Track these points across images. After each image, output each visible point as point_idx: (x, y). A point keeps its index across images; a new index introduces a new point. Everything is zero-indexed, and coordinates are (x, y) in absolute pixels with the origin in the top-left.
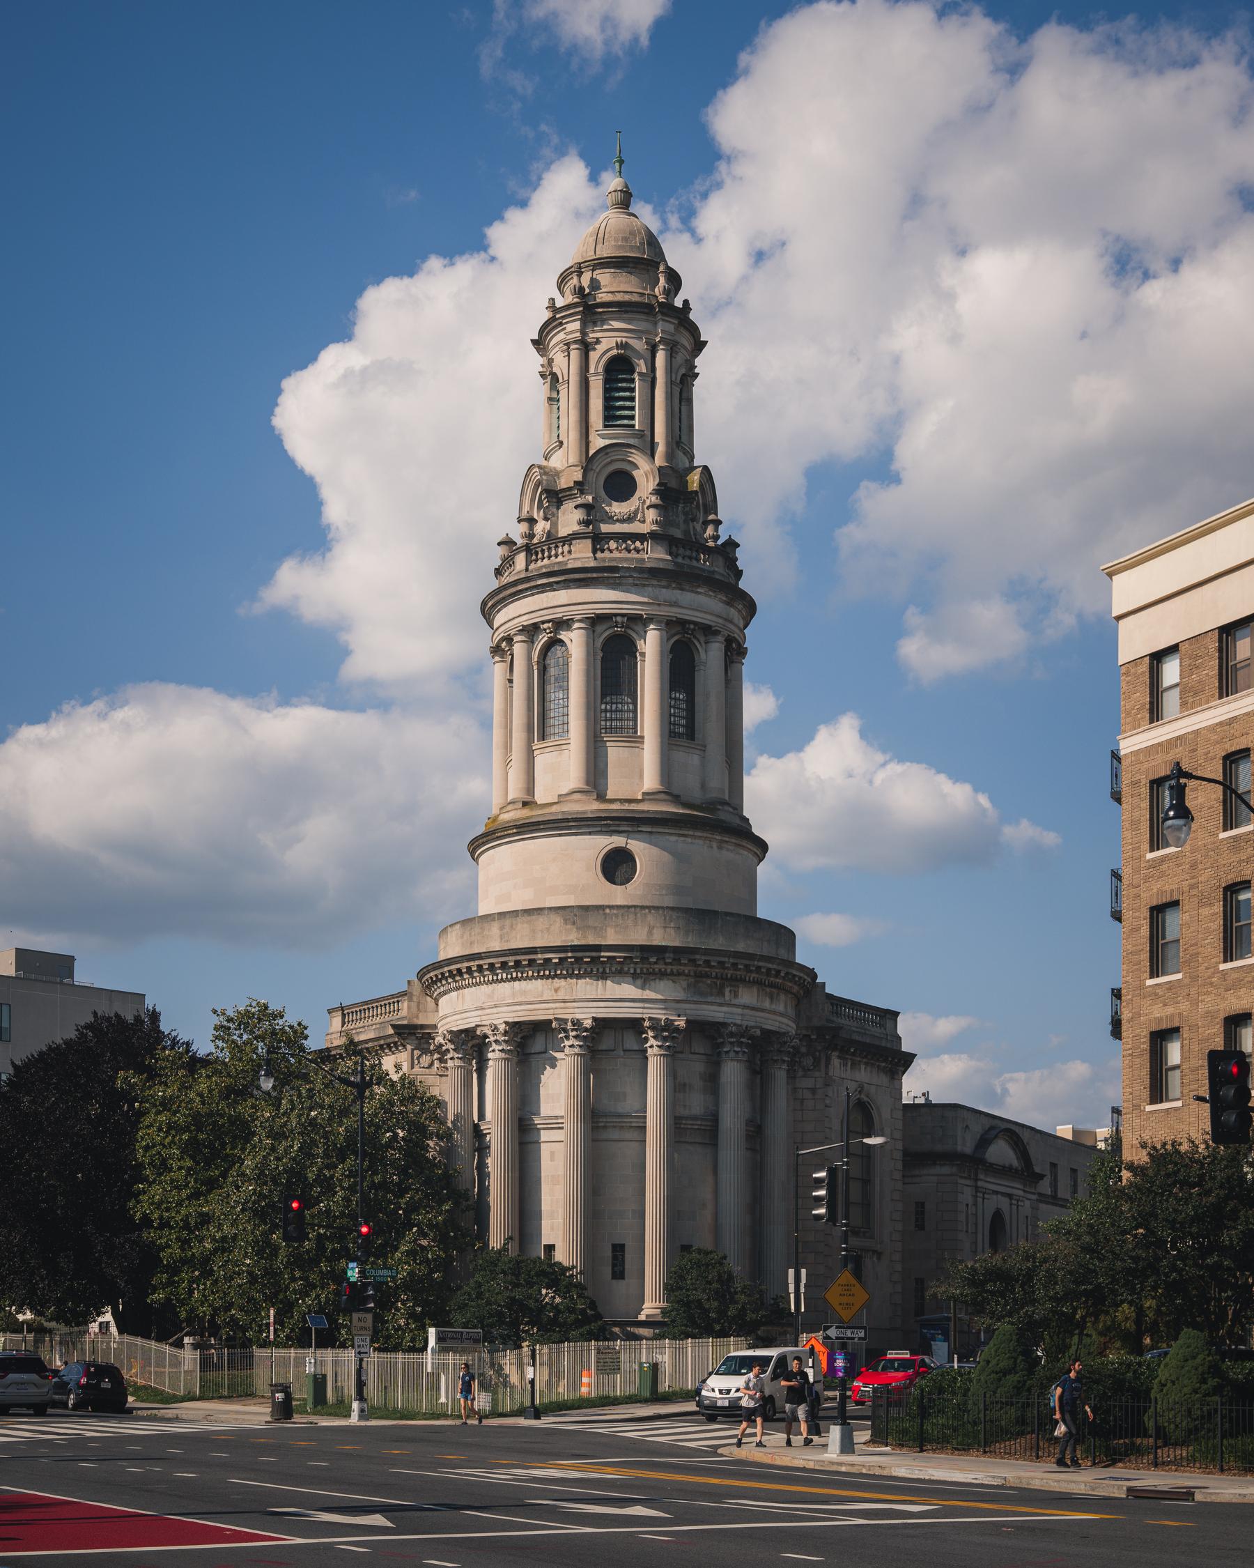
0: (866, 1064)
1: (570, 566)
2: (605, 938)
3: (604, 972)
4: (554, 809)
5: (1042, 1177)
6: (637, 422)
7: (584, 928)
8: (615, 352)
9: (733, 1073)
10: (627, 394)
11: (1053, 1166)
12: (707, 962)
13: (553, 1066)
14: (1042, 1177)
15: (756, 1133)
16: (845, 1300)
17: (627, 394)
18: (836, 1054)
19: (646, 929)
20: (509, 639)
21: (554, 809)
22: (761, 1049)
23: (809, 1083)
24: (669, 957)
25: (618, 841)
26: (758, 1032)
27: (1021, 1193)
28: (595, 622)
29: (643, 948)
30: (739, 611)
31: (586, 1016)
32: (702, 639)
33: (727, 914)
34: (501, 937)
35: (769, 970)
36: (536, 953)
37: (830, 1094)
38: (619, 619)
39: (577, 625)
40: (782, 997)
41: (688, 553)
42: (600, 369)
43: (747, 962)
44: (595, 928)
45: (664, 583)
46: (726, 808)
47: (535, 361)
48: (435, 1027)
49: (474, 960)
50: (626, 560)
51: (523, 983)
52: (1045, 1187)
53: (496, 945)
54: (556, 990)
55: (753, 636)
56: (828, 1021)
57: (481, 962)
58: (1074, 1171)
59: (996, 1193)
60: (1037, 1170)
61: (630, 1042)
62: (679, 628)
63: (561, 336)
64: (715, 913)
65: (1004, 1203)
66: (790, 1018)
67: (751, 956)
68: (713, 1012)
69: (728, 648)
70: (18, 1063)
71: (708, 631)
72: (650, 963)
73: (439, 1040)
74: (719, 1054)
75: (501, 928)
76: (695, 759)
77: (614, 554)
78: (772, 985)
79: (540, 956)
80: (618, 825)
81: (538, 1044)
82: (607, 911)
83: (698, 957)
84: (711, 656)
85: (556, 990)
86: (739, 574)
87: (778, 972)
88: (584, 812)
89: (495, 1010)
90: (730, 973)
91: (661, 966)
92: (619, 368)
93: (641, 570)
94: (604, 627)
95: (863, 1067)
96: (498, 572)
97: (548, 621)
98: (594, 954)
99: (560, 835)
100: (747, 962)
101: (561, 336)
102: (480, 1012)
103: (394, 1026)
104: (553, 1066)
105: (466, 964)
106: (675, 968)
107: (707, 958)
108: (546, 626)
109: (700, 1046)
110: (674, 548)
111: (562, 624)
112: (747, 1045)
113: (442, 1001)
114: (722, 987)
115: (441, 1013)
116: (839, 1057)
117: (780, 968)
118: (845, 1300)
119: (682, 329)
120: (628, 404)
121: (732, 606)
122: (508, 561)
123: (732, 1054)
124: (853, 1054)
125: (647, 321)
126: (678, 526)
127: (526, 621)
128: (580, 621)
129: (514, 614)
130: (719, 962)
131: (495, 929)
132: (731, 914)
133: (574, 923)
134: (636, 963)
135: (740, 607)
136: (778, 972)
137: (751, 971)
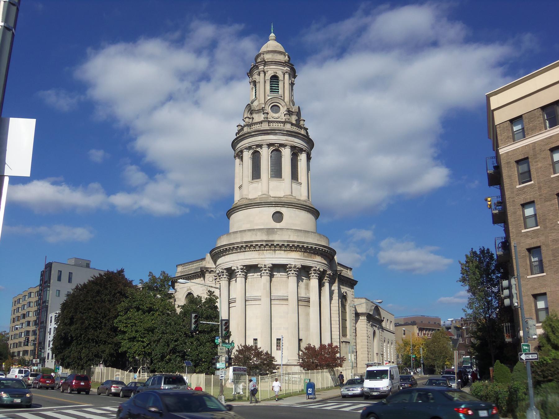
6: (280, 93)
20: (242, 152)
25: (278, 209)
28: (269, 145)
31: (299, 264)
42: (269, 78)
55: (313, 153)
71: (301, 150)
77: (274, 126)
84: (303, 157)
92: (274, 78)
112: (319, 274)
122: (239, 131)
127: (247, 145)
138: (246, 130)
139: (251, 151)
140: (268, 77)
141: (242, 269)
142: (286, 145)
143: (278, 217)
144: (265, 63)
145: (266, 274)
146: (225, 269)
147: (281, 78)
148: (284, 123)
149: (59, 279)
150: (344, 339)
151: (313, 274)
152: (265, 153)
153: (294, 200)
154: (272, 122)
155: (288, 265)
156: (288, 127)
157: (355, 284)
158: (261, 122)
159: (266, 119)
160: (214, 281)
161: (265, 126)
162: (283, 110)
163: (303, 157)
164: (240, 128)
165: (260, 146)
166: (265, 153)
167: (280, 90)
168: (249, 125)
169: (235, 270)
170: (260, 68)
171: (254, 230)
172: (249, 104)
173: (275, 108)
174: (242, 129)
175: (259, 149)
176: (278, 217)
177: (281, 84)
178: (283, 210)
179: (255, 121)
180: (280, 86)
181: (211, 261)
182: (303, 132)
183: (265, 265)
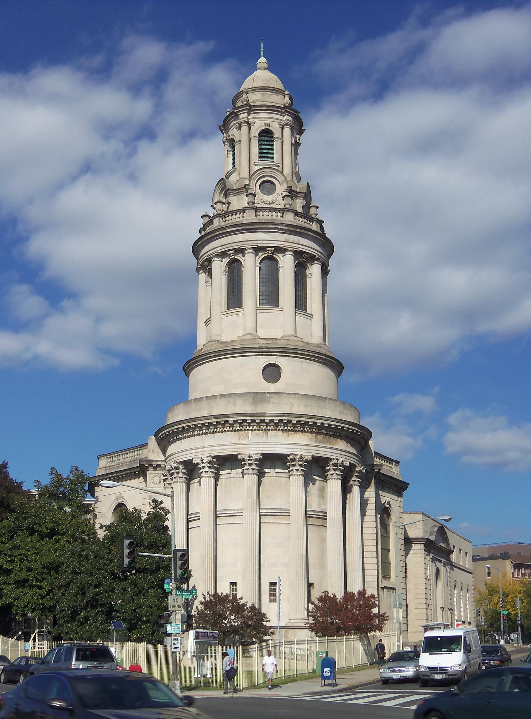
4: (279, 342)
8: (264, 128)
10: (270, 147)
13: (314, 484)
17: (270, 147)
20: (209, 261)
21: (279, 342)
25: (272, 360)
28: (257, 250)
31: (308, 454)
36: (228, 417)
39: (289, 253)
42: (257, 135)
53: (205, 413)
68: (323, 452)
70: (141, 479)
77: (266, 216)
79: (231, 419)
82: (268, 395)
84: (314, 271)
89: (203, 449)
92: (266, 135)
97: (232, 250)
98: (262, 418)
99: (256, 355)
102: (194, 451)
104: (314, 484)
111: (242, 251)
120: (270, 152)
127: (219, 250)
128: (291, 251)
131: (205, 404)
138: (217, 223)
139: (226, 260)
141: (210, 462)
142: (286, 250)
143: (272, 373)
144: (250, 109)
145: (251, 471)
146: (181, 463)
147: (277, 133)
148: (282, 211)
150: (385, 583)
151: (332, 472)
152: (250, 264)
155: (288, 455)
156: (289, 218)
157: (404, 489)
158: (243, 211)
159: (251, 205)
160: (162, 484)
161: (250, 217)
162: (281, 189)
164: (207, 219)
165: (242, 251)
166: (250, 264)
167: (275, 156)
168: (223, 215)
169: (198, 464)
170: (241, 116)
171: (230, 395)
172: (222, 179)
173: (268, 186)
174: (211, 222)
175: (239, 257)
176: (272, 373)
177: (277, 145)
179: (232, 208)
180: (275, 148)
181: (158, 449)
182: (314, 227)
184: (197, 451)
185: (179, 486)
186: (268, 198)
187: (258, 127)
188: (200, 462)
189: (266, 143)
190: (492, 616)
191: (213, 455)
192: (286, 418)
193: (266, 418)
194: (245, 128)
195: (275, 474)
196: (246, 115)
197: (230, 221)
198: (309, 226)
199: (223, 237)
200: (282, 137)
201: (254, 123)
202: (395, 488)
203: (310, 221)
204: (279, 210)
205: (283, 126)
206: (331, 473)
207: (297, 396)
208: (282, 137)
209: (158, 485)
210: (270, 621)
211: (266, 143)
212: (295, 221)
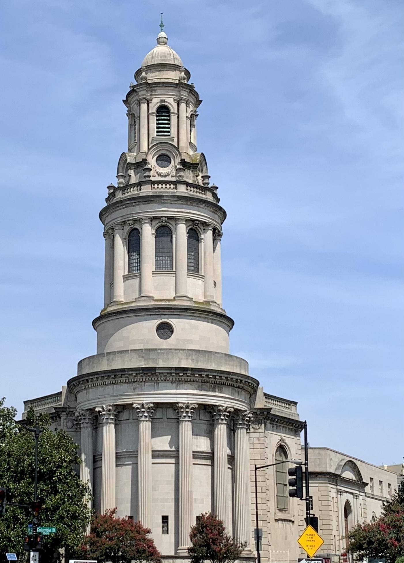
0: (283, 427)
1: (140, 195)
2: (158, 364)
3: (157, 380)
4: (133, 305)
5: (367, 484)
7: (147, 359)
8: (159, 104)
9: (221, 431)
11: (371, 479)
12: (207, 375)
14: (367, 484)
15: (232, 459)
16: (310, 543)
18: (269, 421)
19: (178, 360)
21: (133, 305)
22: (234, 419)
23: (256, 435)
24: (189, 373)
26: (233, 410)
27: (358, 492)
29: (176, 369)
30: (219, 216)
32: (202, 228)
33: (216, 353)
34: (108, 364)
35: (237, 380)
37: (267, 441)
38: (164, 218)
40: (243, 393)
41: (195, 190)
42: (155, 111)
43: (226, 376)
44: (153, 359)
45: (184, 203)
46: (215, 304)
47: (125, 109)
48: (75, 408)
49: (94, 375)
50: (167, 192)
51: (119, 386)
52: (367, 489)
54: (134, 389)
55: (226, 227)
56: (265, 405)
57: (98, 376)
58: (381, 482)
59: (346, 492)
60: (364, 481)
61: (171, 413)
62: (192, 223)
63: (136, 98)
64: (211, 352)
65: (350, 497)
66: (246, 404)
67: (229, 373)
69: (214, 232)
71: (204, 224)
72: (180, 376)
73: (77, 414)
74: (213, 420)
75: (108, 360)
76: (200, 282)
77: (161, 189)
78: (238, 387)
80: (164, 312)
81: (125, 415)
82: (159, 351)
83: (202, 373)
84: (207, 236)
85: (134, 389)
86: (218, 200)
87: (241, 381)
88: (148, 306)
90: (218, 381)
91: (185, 377)
92: (163, 110)
93: (174, 197)
94: (157, 222)
95: (281, 428)
96: (107, 200)
99: (136, 316)
100: (226, 376)
101: (136, 98)
102: (97, 401)
103: (55, 408)
105: (91, 377)
106: (192, 378)
107: (208, 373)
108: (130, 222)
109: (203, 416)
110: (189, 188)
112: (227, 416)
113: (79, 396)
114: (215, 387)
115: (78, 402)
116: (270, 423)
117: (242, 379)
118: (310, 543)
119: (191, 94)
121: (216, 214)
122: (112, 195)
123: (220, 421)
124: (277, 422)
125: (176, 91)
126: (190, 179)
127: (119, 220)
129: (118, 215)
130: (213, 376)
132: (219, 353)
133: (143, 357)
134: (173, 376)
135: (219, 214)
136: (241, 381)
137: (228, 380)
138: (120, 196)
139: (127, 229)
140: (153, 109)
143: (165, 330)
144: (152, 86)
146: (88, 410)
148: (176, 183)
149: (165, 519)
150: (280, 515)
152: (148, 233)
153: (153, 303)
154: (158, 182)
163: (207, 236)
166: (148, 233)
169: (100, 412)
170: (140, 93)
175: (136, 226)
176: (165, 330)
177: (174, 119)
178: (173, 322)
182: (208, 196)
183: (143, 405)
184: (99, 400)
185: (86, 432)
186: (164, 171)
187: (155, 103)
188: (101, 410)
189: (163, 118)
190: (46, 543)
191: (199, 402)
192: (174, 371)
193: (157, 371)
194: (144, 106)
195: (166, 420)
196: (145, 92)
197: (130, 194)
198: (204, 197)
199: (123, 208)
200: (178, 111)
201: (152, 100)
202: (291, 427)
203: (202, 190)
204: (170, 182)
205: (178, 101)
206: (217, 418)
207: (185, 351)
208: (178, 111)
209: (71, 430)
210: (314, 541)
211: (163, 118)
212: (186, 191)
